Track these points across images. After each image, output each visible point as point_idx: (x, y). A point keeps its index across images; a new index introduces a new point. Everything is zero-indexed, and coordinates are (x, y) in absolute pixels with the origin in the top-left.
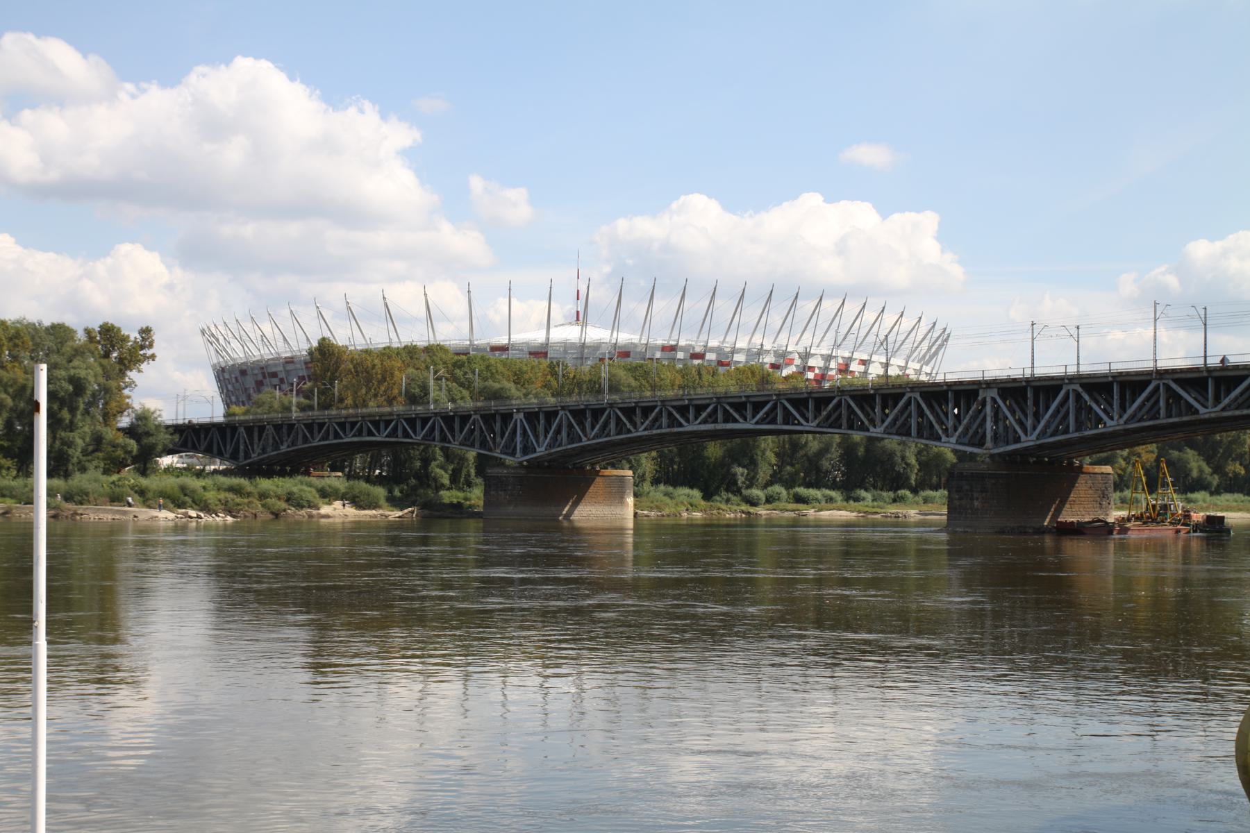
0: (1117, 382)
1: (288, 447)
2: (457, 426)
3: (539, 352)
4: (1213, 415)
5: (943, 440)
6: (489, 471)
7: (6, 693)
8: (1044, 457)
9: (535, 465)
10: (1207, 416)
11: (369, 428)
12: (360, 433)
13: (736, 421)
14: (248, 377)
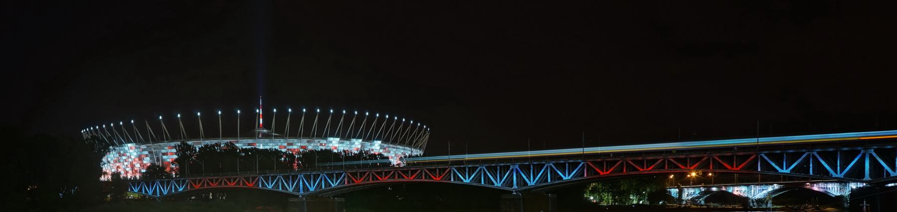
2: (251, 181)
8: (709, 173)
13: (403, 177)
14: (121, 166)
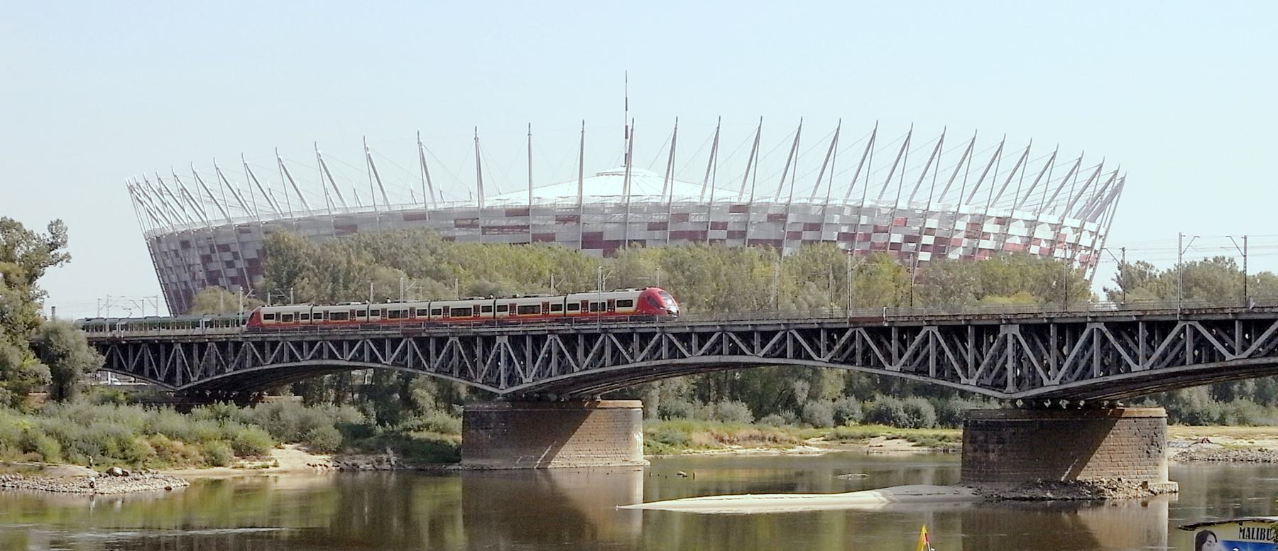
0: (1143, 322)
1: (234, 370)
10: (1233, 364)
11: (330, 350)
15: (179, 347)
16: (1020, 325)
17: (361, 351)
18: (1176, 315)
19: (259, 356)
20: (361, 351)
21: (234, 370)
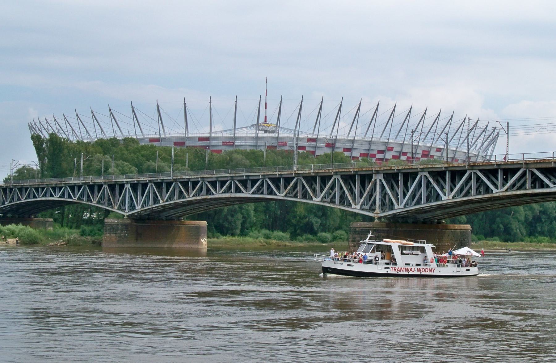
0: (449, 171)
1: (10, 202)
3: (180, 143)
4: (501, 194)
5: (353, 207)
6: (106, 221)
7: (554, 277)
9: (138, 219)
10: (497, 195)
11: (237, 186)
12: (45, 195)
15: (106, 186)
16: (384, 174)
17: (64, 192)
18: (466, 166)
19: (20, 196)
20: (46, 193)
21: (10, 202)
